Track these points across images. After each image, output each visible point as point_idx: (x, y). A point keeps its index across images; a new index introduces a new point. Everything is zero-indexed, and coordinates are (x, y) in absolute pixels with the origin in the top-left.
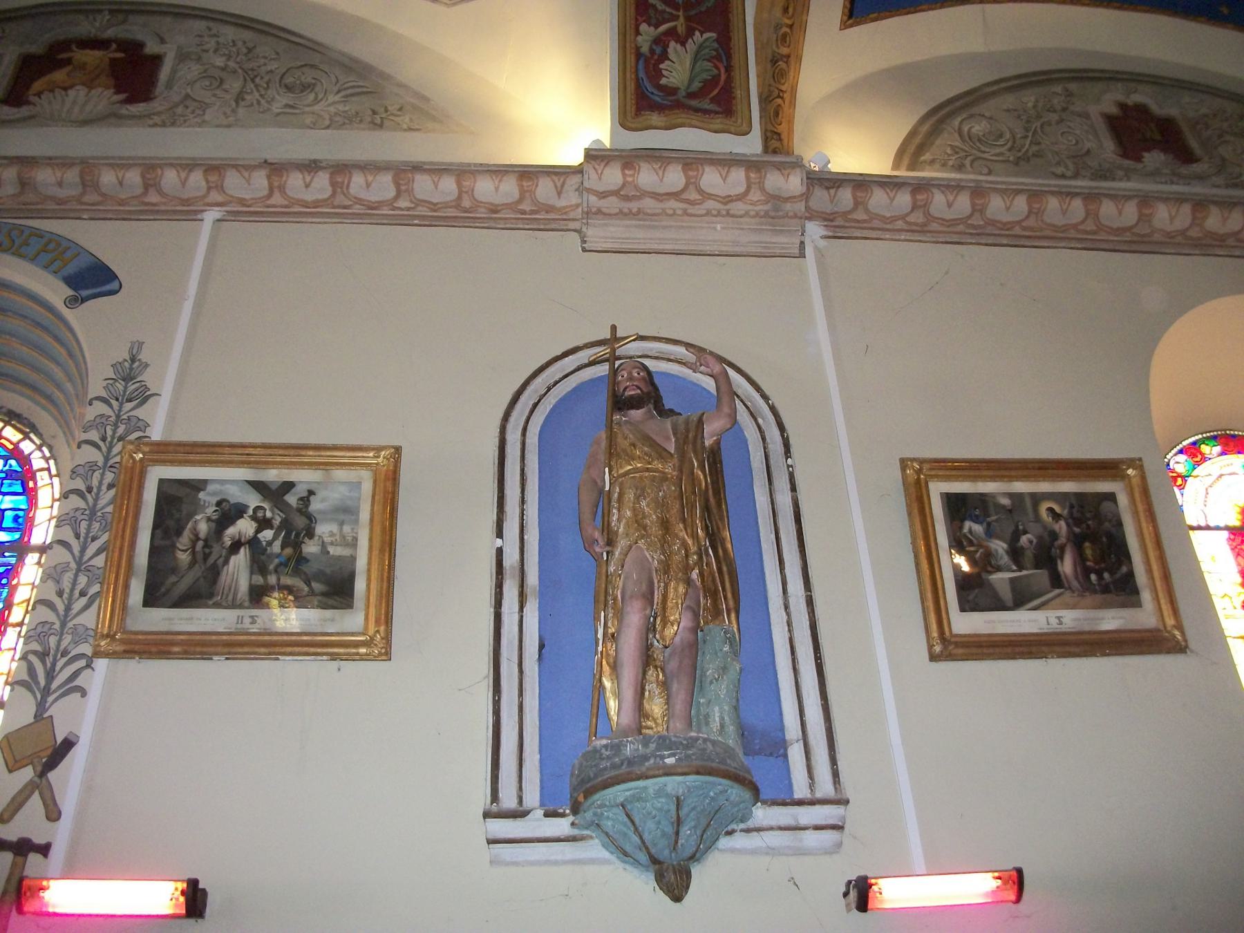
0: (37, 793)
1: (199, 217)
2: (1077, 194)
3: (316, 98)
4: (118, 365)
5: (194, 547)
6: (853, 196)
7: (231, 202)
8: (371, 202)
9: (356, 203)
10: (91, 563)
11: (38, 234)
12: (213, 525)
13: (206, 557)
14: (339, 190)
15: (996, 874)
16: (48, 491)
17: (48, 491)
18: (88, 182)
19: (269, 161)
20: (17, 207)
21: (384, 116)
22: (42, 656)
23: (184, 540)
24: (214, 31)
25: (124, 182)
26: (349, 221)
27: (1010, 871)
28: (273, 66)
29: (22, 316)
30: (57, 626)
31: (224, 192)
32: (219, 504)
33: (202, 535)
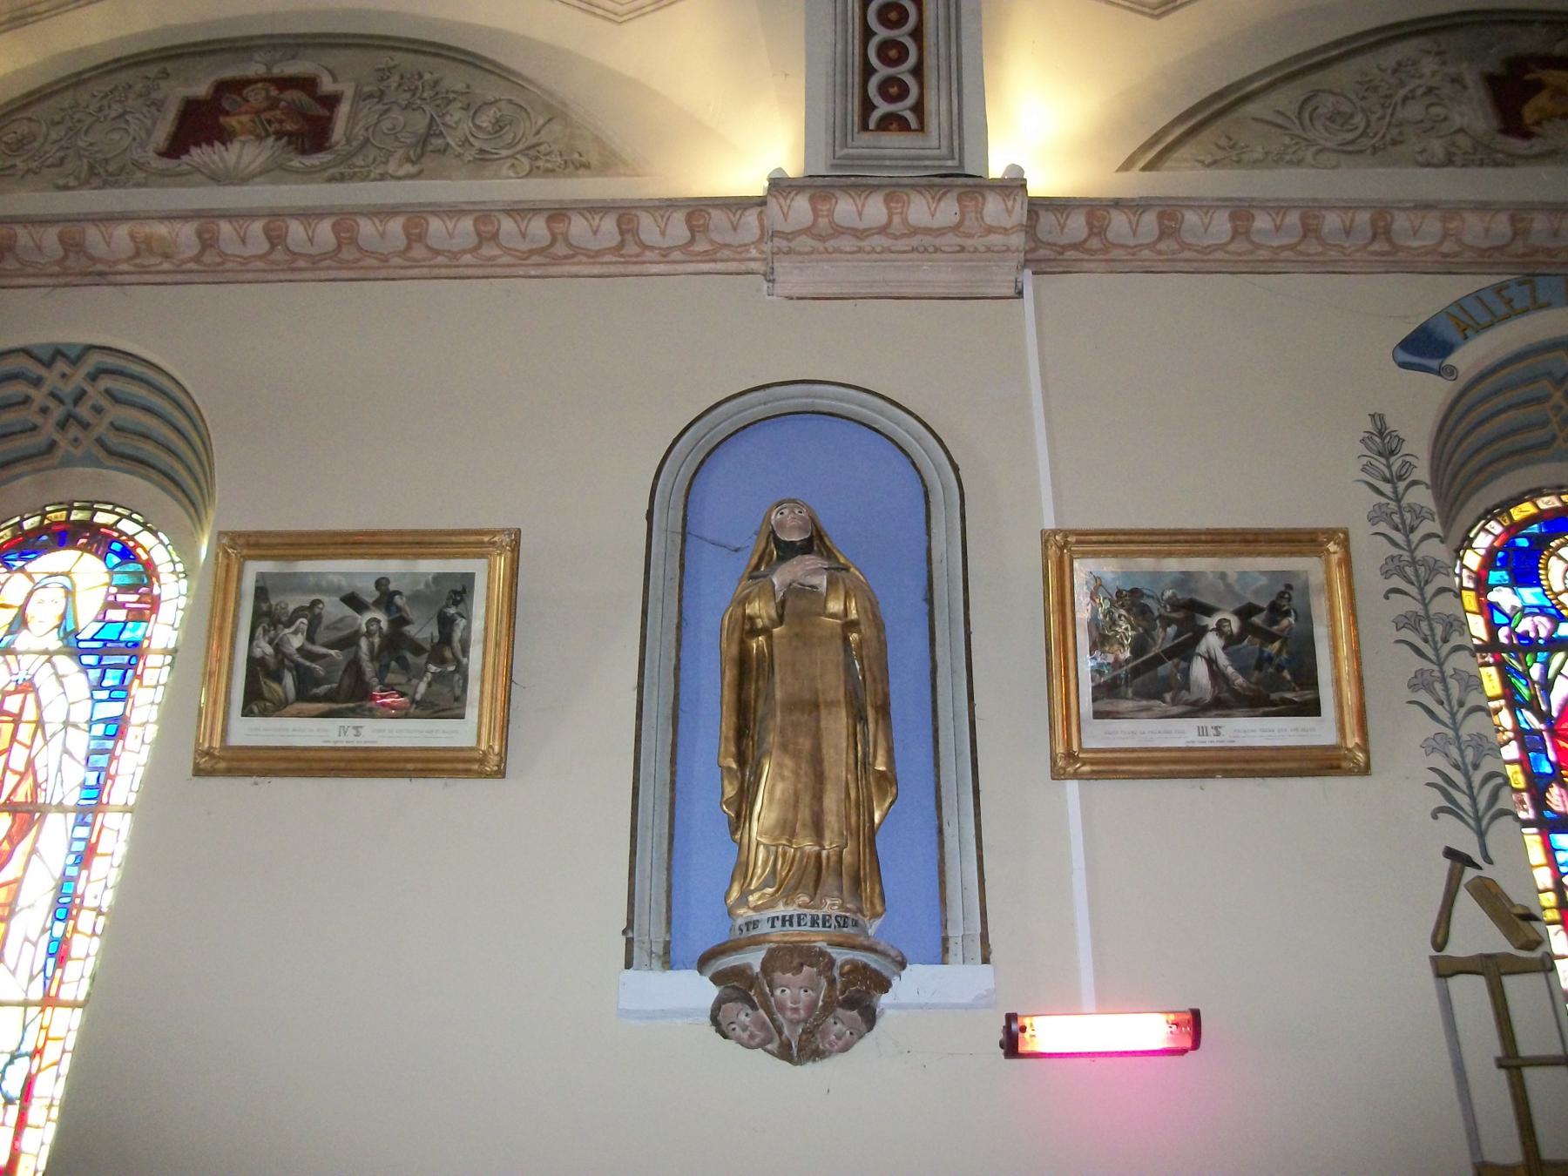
2: (536, 211)
6: (1087, 222)
15: (1172, 1017)
16: (173, 590)
17: (173, 590)
18: (415, 236)
25: (315, 239)
27: (1184, 1012)
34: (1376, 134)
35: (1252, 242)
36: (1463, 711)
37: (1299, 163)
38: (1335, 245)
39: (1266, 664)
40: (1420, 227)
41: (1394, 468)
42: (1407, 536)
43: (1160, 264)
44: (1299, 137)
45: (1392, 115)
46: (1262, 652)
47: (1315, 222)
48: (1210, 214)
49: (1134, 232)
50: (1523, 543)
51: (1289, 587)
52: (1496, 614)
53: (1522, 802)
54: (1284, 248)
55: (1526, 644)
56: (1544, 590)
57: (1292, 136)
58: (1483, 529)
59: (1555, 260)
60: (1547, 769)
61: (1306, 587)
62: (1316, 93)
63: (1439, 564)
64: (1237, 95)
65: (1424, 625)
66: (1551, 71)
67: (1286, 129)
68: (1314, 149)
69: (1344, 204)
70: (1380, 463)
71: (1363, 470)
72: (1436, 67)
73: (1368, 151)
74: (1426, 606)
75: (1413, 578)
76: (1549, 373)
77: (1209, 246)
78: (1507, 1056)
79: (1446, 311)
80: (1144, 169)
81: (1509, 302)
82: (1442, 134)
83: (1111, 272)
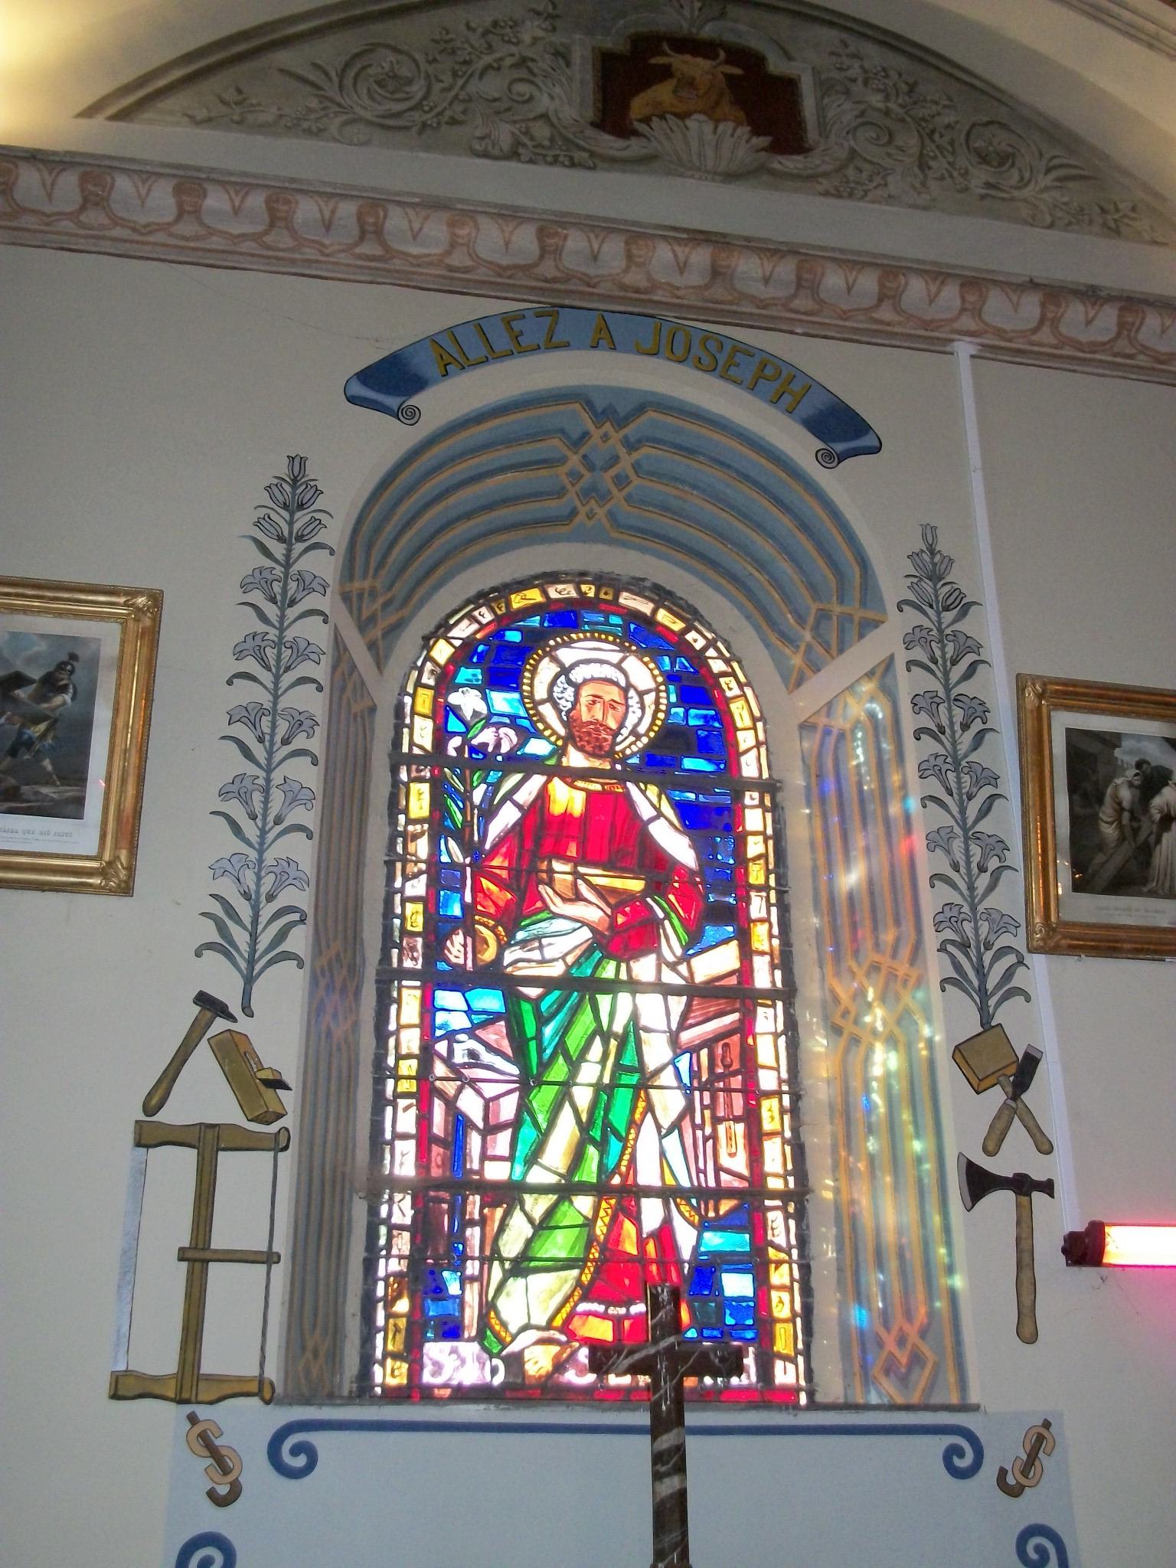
0: (1016, 1117)
1: (948, 349)
3: (1022, 179)
4: (946, 560)
5: (1119, 819)
7: (986, 332)
8: (1158, 352)
9: (1141, 352)
10: (977, 829)
11: (749, 351)
12: (1137, 792)
13: (1136, 831)
14: (1125, 333)
19: (1036, 280)
20: (700, 304)
21: (1116, 216)
22: (964, 946)
23: (1107, 812)
24: (852, 49)
26: (1134, 377)
28: (949, 118)
29: (722, 464)
30: (966, 909)
31: (980, 317)
32: (1139, 765)
33: (1126, 804)
34: (431, 109)
35: (202, 224)
36: (279, 829)
37: (318, 133)
38: (313, 241)
39: (23, 749)
40: (421, 229)
41: (297, 526)
42: (282, 610)
43: (82, 241)
44: (331, 100)
45: (463, 87)
46: (20, 734)
47: (285, 208)
48: (150, 182)
49: (50, 196)
50: (514, 636)
51: (73, 657)
52: (452, 718)
53: (413, 949)
54: (244, 236)
55: (479, 759)
56: (522, 697)
57: (324, 98)
58: (469, 616)
59: (595, 291)
60: (456, 910)
61: (94, 662)
62: (372, 48)
63: (312, 648)
64: (269, 38)
65: (265, 723)
66: (688, 58)
67: (319, 88)
68: (345, 117)
69: (329, 190)
70: (281, 518)
71: (257, 524)
72: (541, 33)
73: (415, 129)
74: (276, 698)
75: (272, 663)
76: (562, 431)
77: (148, 225)
78: (194, 1246)
79: (433, 340)
80: (115, 117)
81: (516, 338)
82: (516, 118)
83: (14, 244)
